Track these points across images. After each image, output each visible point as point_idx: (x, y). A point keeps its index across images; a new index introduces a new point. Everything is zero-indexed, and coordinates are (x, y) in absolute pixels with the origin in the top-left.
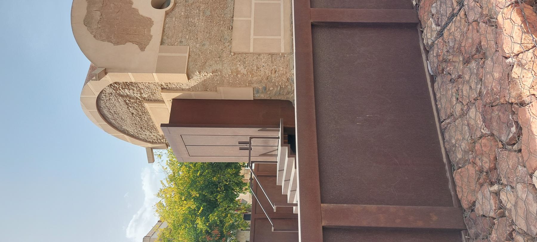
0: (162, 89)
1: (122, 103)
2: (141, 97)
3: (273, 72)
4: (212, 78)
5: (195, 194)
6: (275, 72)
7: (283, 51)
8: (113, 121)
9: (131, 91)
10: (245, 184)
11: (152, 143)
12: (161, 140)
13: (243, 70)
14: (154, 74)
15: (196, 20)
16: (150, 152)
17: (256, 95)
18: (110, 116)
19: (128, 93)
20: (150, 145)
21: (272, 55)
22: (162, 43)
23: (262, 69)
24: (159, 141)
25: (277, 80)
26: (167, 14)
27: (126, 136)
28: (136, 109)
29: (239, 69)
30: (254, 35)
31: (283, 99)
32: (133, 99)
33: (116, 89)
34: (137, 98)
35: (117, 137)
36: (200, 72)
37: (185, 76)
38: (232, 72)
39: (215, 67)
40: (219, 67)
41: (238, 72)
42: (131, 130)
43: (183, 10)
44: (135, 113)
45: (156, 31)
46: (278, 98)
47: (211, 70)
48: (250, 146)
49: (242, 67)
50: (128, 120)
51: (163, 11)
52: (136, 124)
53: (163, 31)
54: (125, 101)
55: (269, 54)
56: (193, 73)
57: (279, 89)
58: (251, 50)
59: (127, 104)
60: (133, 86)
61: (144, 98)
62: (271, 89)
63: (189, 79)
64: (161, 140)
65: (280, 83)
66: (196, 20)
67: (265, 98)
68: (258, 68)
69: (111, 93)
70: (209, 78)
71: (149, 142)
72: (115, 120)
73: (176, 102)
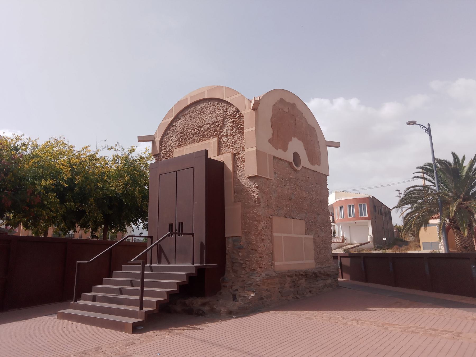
0: (235, 154)
1: (215, 120)
2: (223, 135)
3: (261, 255)
4: (251, 198)
5: (79, 179)
6: (260, 257)
7: (276, 263)
8: (191, 110)
9: (230, 128)
10: (66, 231)
11: (161, 141)
12: (165, 149)
13: (262, 226)
14: (255, 149)
15: (288, 187)
16: (151, 139)
17: (230, 239)
18: (198, 107)
19: (226, 126)
20: (158, 139)
21: (272, 254)
22: (274, 157)
23: (262, 244)
24: (163, 148)
25: (253, 260)
26: (290, 163)
27: (170, 120)
28: (207, 130)
29: (261, 223)
30: (284, 237)
31: (227, 266)
32: (220, 129)
33: (232, 116)
34: (221, 132)
35: (171, 111)
36: (257, 187)
37: (254, 173)
38: (259, 216)
39: (262, 201)
40: (262, 205)
41: (259, 221)
42: (180, 123)
43: (293, 177)
44: (202, 129)
45: (279, 153)
46: (227, 261)
47: (260, 197)
48: (176, 234)
49: (263, 225)
50: (193, 123)
51: (291, 160)
52: (187, 129)
53: (280, 159)
54: (218, 122)
55: (273, 251)
56: (257, 182)
57: (240, 262)
58: (275, 234)
59: (214, 123)
60: (236, 130)
61: (221, 138)
62: (240, 254)
63: (249, 178)
64: (165, 149)
65: (248, 263)
66: (288, 187)
67: (227, 249)
68: (263, 240)
69: (227, 111)
70: (251, 195)
71: (162, 139)
72: (193, 112)
73: (221, 165)
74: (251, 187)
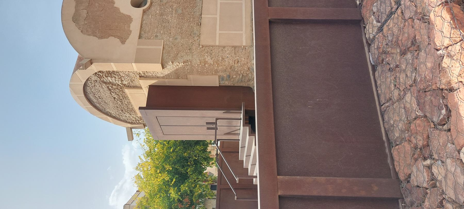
0: (140, 77)
1: (106, 89)
2: (122, 84)
3: (236, 62)
4: (183, 68)
5: (168, 167)
6: (238, 62)
7: (244, 44)
8: (98, 105)
9: (113, 78)
10: (212, 159)
11: (132, 123)
12: (139, 121)
13: (210, 60)
14: (133, 64)
15: (169, 17)
16: (130, 131)
17: (221, 82)
18: (95, 100)
19: (111, 81)
20: (130, 125)
21: (235, 47)
22: (140, 37)
23: (226, 59)
24: (138, 122)
25: (240, 69)
26: (144, 12)
27: (108, 117)
28: (118, 95)
29: (207, 60)
30: (220, 30)
31: (244, 85)
32: (115, 85)
33: (100, 77)
34: (118, 85)
35: (101, 118)
36: (172, 63)
37: (160, 65)
38: (200, 63)
39: (185, 58)
40: (189, 58)
41: (206, 63)
42: (113, 112)
43: (159, 9)
44: (116, 98)
45: (135, 27)
46: (240, 85)
47: (182, 60)
48: (216, 126)
49: (209, 58)
50: (111, 104)
51: (141, 10)
52: (117, 107)
53: (141, 27)
54: (108, 87)
55: (233, 47)
56: (167, 63)
57: (241, 77)
58: (217, 44)
59: (110, 90)
60: (115, 74)
61: (125, 85)
62: (234, 77)
63: (163, 68)
64: (139, 121)
65: (242, 72)
66: (169, 17)
67: (229, 85)
68: (223, 59)
69: (96, 81)
70: (181, 67)
71: (129, 123)
72: (100, 103)
73: (152, 88)
74: (171, 68)
